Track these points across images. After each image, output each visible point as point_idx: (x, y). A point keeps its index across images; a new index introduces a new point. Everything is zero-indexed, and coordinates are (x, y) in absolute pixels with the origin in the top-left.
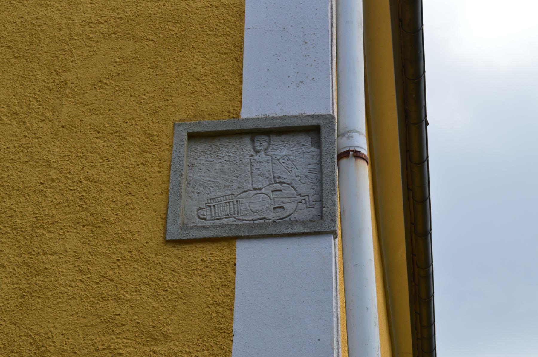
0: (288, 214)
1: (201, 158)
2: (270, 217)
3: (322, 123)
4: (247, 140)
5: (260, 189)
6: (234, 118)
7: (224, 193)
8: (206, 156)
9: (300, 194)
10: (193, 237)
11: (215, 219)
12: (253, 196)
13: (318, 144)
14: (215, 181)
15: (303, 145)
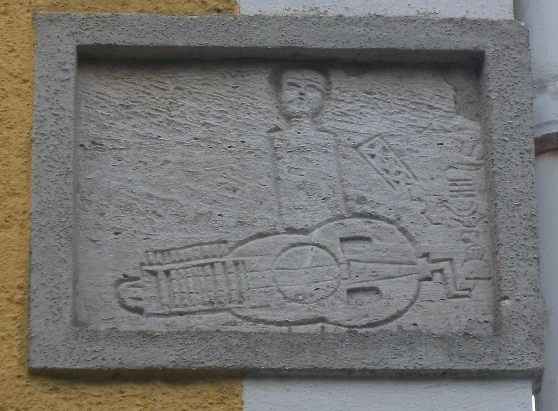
0: (392, 311)
1: (120, 125)
2: (340, 316)
3: (488, 44)
4: (258, 83)
5: (305, 231)
6: (219, 11)
7: (196, 237)
8: (135, 121)
9: (426, 255)
10: (114, 365)
11: (172, 314)
12: (285, 250)
13: (476, 106)
14: (169, 196)
15: (430, 107)
